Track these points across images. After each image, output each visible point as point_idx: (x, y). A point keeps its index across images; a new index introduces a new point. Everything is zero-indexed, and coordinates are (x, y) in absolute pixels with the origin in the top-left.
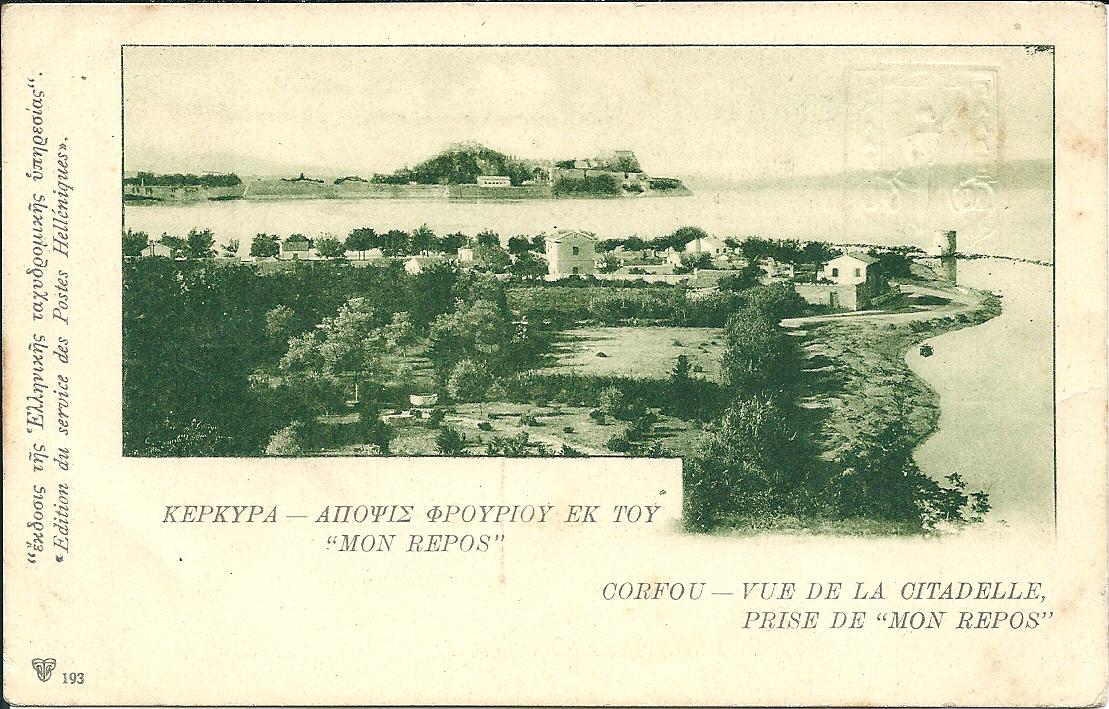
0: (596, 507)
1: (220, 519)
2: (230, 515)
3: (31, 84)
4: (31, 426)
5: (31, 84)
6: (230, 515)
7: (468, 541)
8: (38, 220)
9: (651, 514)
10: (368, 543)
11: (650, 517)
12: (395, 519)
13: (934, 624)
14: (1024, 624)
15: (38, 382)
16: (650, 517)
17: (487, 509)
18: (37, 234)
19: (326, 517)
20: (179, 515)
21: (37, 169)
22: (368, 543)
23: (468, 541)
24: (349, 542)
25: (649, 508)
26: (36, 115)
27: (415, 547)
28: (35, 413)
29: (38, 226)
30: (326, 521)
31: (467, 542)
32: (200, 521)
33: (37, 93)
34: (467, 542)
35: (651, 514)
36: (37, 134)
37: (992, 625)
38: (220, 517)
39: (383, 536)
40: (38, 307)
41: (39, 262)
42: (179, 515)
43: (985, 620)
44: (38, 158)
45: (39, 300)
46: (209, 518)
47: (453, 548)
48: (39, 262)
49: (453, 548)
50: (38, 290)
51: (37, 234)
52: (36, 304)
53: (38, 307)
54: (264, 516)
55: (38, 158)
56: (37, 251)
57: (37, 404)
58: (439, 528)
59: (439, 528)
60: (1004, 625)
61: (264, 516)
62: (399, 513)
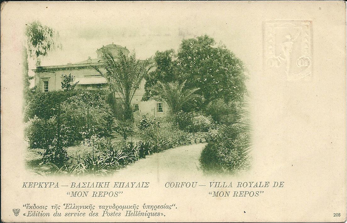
0: (135, 183)
1: (40, 186)
2: (44, 185)
3: (173, 205)
4: (66, 205)
5: (173, 205)
6: (44, 185)
7: (252, 193)
8: (130, 207)
9: (46, 185)
10: (222, 194)
11: (132, 186)
12: (143, 186)
13: (227, 195)
14: (114, 195)
15: (80, 208)
16: (132, 186)
17: (133, 184)
18: (126, 207)
19: (257, 186)
20: (27, 185)
21: (146, 207)
22: (222, 194)
23: (252, 193)
24: (216, 194)
25: (132, 183)
26: (163, 207)
27: (235, 195)
28: (70, 207)
29: (128, 207)
30: (79, 187)
31: (111, 194)
32: (104, 196)
33: (170, 207)
34: (111, 194)
35: (46, 185)
36: (158, 207)
37: (103, 196)
38: (40, 186)
39: (226, 192)
40: (103, 207)
41: (117, 208)
42: (27, 185)
43: (242, 194)
44: (150, 207)
45: (105, 208)
46: (37, 186)
47: (107, 196)
48: (117, 208)
49: (107, 196)
50: (109, 207)
51: (126, 207)
52: (104, 207)
53: (103, 207)
54: (54, 186)
55: (150, 207)
56: (121, 207)
57: (73, 207)
58: (242, 189)
59: (242, 189)
60: (247, 195)
61: (54, 186)
62: (145, 185)
